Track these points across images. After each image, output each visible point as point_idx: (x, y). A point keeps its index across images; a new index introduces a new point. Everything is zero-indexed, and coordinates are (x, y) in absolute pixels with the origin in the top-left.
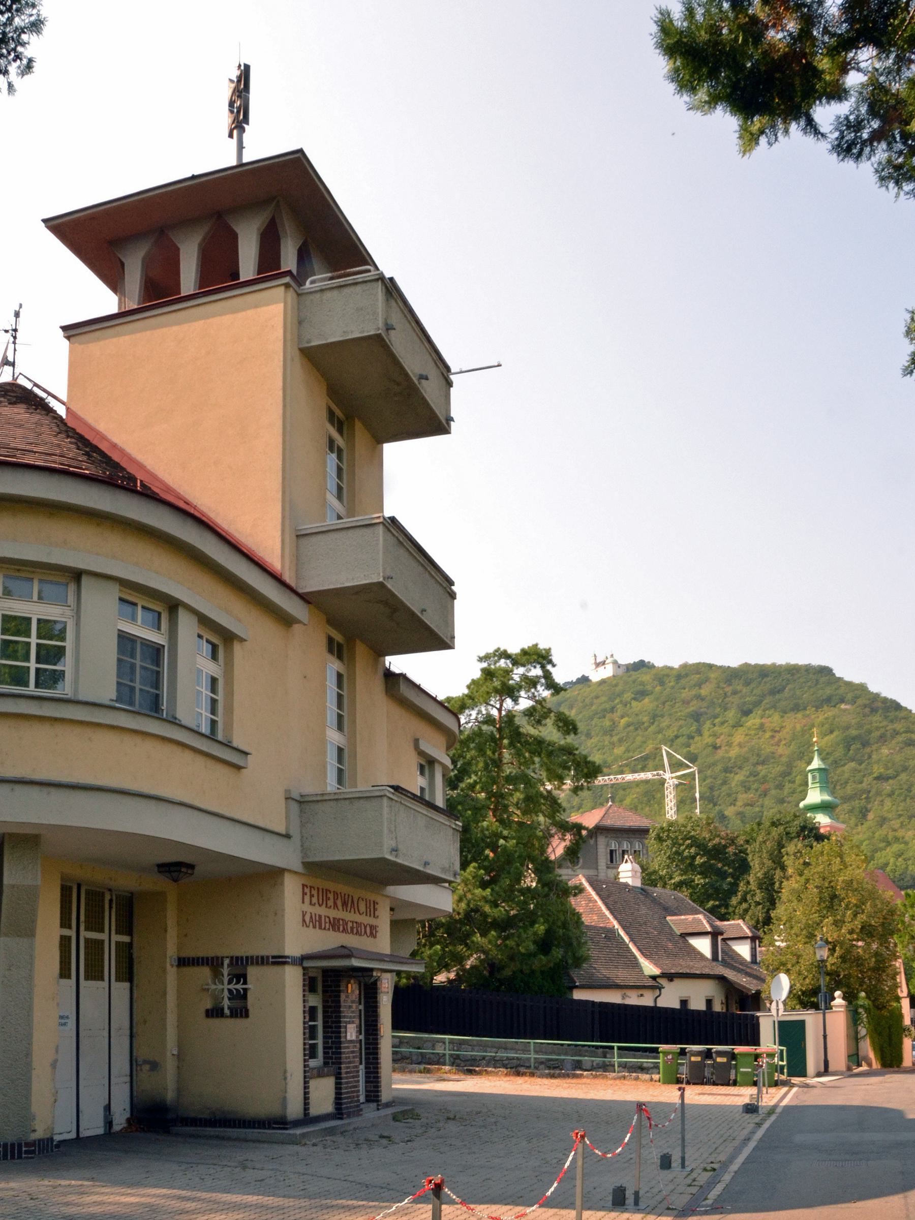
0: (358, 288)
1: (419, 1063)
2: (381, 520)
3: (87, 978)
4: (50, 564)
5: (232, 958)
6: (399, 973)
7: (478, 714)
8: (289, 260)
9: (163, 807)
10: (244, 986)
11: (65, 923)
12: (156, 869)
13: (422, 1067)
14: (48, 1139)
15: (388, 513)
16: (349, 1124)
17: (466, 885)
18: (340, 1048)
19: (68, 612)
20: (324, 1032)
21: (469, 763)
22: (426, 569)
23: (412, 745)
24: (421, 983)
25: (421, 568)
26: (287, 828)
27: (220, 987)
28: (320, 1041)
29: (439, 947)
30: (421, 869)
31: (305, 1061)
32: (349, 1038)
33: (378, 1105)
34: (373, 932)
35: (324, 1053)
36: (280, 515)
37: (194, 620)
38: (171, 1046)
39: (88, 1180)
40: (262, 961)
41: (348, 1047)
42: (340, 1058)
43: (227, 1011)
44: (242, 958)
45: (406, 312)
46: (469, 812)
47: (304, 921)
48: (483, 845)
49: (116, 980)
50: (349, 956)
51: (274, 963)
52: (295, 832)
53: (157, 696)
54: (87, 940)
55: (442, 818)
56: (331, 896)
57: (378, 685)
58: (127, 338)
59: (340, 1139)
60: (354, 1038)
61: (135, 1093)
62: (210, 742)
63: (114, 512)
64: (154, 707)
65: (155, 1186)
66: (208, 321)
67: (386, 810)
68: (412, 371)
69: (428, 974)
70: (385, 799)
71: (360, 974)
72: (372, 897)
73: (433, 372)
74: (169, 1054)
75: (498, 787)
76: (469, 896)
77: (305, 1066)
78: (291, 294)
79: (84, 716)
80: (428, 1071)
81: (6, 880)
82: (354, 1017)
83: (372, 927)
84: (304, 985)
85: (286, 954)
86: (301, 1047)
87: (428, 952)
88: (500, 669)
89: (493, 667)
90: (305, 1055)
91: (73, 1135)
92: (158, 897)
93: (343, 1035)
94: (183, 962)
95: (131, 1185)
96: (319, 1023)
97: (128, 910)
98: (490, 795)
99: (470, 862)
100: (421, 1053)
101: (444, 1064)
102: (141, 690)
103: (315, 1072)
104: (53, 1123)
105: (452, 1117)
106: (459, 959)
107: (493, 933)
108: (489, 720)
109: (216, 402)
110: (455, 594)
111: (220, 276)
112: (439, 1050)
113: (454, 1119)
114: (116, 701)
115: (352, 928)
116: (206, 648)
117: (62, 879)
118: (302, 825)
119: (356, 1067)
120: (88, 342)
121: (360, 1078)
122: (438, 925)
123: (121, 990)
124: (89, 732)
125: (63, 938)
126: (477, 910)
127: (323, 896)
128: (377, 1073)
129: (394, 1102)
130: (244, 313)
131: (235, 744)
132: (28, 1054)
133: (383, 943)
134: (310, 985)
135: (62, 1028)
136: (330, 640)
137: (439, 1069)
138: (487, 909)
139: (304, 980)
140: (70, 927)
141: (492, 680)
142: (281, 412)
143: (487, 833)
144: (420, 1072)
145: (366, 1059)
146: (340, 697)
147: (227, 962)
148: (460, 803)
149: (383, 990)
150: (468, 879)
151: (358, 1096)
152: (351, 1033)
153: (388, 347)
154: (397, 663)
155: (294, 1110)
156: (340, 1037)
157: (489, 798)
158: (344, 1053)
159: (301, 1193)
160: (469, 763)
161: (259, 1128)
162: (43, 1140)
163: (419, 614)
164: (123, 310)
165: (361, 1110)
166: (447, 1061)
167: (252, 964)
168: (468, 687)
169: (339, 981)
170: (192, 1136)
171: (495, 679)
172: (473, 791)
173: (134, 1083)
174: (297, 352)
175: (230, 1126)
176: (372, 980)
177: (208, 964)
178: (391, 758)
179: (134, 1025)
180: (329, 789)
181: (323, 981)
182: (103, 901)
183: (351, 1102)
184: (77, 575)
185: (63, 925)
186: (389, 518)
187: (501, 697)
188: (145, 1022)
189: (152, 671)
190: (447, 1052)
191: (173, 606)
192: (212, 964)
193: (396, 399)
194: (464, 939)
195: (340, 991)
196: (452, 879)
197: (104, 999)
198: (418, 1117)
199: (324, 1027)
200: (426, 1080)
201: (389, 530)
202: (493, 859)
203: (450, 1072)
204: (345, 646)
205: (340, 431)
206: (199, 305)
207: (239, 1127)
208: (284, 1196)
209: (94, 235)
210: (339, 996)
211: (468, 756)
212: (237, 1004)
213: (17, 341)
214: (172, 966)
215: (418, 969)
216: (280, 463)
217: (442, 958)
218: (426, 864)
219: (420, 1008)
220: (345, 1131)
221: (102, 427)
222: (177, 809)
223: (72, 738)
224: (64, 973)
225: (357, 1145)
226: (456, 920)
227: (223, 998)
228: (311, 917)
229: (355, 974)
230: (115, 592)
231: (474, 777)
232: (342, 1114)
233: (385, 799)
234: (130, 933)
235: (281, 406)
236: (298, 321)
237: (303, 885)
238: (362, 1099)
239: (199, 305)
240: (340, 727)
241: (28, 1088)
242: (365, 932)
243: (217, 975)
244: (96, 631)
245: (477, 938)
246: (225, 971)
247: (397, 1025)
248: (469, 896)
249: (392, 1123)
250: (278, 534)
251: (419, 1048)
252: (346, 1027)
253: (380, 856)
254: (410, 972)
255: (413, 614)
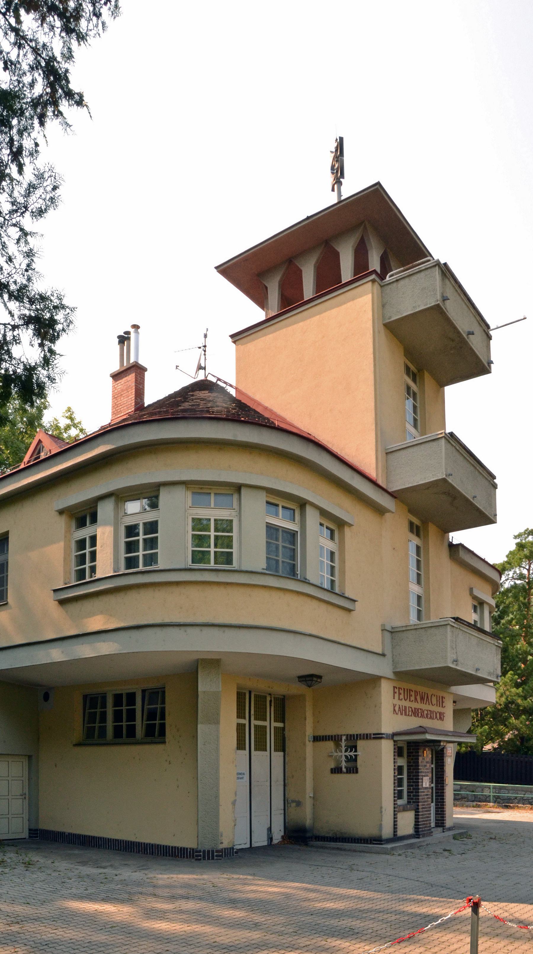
0: (423, 274)
1: (473, 801)
2: (443, 435)
3: (256, 749)
4: (221, 482)
5: (347, 735)
6: (460, 744)
7: (514, 574)
8: (375, 264)
9: (299, 637)
10: (355, 753)
11: (240, 714)
12: (297, 679)
13: (475, 803)
14: (230, 848)
15: (448, 431)
16: (424, 841)
17: (506, 686)
18: (418, 792)
19: (234, 513)
20: (408, 782)
21: (508, 607)
22: (476, 468)
23: (468, 593)
24: (475, 750)
25: (472, 468)
26: (383, 649)
27: (340, 754)
28: (405, 788)
29: (487, 727)
30: (474, 673)
31: (395, 801)
32: (424, 786)
33: (443, 829)
34: (441, 716)
35: (408, 796)
36: (374, 440)
37: (317, 513)
38: (309, 792)
39: (251, 875)
40: (367, 737)
41: (424, 792)
42: (418, 799)
43: (344, 770)
44: (354, 735)
45: (457, 287)
46: (508, 639)
47: (394, 710)
48: (517, 659)
49: (275, 751)
50: (424, 733)
51: (374, 738)
52: (388, 652)
53: (294, 565)
54: (256, 726)
55: (488, 639)
56: (413, 694)
57: (445, 553)
58: (271, 336)
59: (417, 851)
60: (428, 786)
61: (287, 820)
62: (329, 594)
63: (260, 443)
64: (292, 572)
65: (293, 881)
66: (322, 315)
67: (449, 634)
68: (462, 329)
69: (479, 744)
70: (449, 627)
71: (432, 744)
72: (441, 694)
73: (477, 330)
74: (307, 796)
75: (527, 621)
76: (508, 693)
77: (394, 804)
78: (376, 286)
79: (248, 582)
80: (479, 806)
81: (200, 689)
82: (428, 772)
83: (440, 713)
84: (394, 752)
85: (382, 732)
86: (392, 792)
87: (479, 730)
88: (529, 542)
89: (524, 541)
90: (394, 797)
91: (248, 846)
92: (300, 698)
93: (420, 784)
94: (316, 739)
95: (278, 879)
96: (405, 776)
97: (282, 706)
98: (522, 626)
99: (509, 671)
100: (474, 795)
101: (489, 802)
102: (283, 562)
103: (401, 808)
104: (234, 839)
105: (494, 837)
106: (501, 735)
107: (523, 716)
108: (521, 577)
109: (328, 371)
110: (497, 485)
111: (330, 283)
112: (486, 793)
113: (495, 839)
114: (266, 569)
115: (427, 714)
116: (326, 533)
117: (238, 688)
118: (393, 647)
119: (429, 804)
120: (247, 343)
121: (432, 812)
122: (487, 713)
123: (278, 757)
124: (248, 591)
125: (238, 725)
126: (512, 702)
127: (408, 694)
128: (443, 808)
129: (454, 827)
130: (345, 305)
131: (346, 595)
132: (217, 797)
133: (448, 724)
134: (399, 752)
135: (240, 780)
136: (411, 524)
137: (486, 805)
138: (519, 701)
139: (395, 749)
140: (245, 718)
141: (523, 550)
142: (373, 369)
143: (520, 652)
144: (474, 807)
145: (436, 799)
146: (418, 562)
147: (344, 738)
148: (501, 633)
149: (448, 754)
150: (507, 682)
151: (430, 823)
152: (426, 782)
153: (445, 313)
154: (457, 537)
155: (387, 832)
156: (418, 785)
157: (521, 629)
158: (421, 796)
159: (387, 888)
160: (508, 607)
161: (364, 843)
162: (228, 849)
163: (471, 500)
164: (268, 317)
165: (432, 832)
166: (492, 800)
167: (360, 739)
168: (507, 556)
169: (418, 749)
170: (322, 847)
171: (525, 549)
172: (510, 625)
173: (286, 815)
174: (382, 328)
175: (345, 842)
176: (441, 748)
177: (332, 740)
178: (452, 600)
179: (286, 779)
180: (412, 623)
181: (408, 749)
182: (266, 702)
183: (425, 827)
184: (238, 488)
185: (239, 717)
186: (449, 433)
187: (529, 561)
188: (293, 776)
189: (290, 549)
190: (492, 794)
191: (303, 504)
192: (335, 740)
193: (452, 352)
194: (504, 722)
195: (418, 756)
196: (495, 680)
197: (267, 763)
198: (470, 837)
199: (408, 779)
200: (477, 812)
201: (449, 442)
202: (524, 669)
203: (493, 807)
204: (421, 528)
205: (414, 380)
206: (316, 305)
207: (352, 842)
208: (375, 891)
209: (249, 272)
210: (418, 759)
211: (507, 602)
212: (350, 765)
213: (206, 353)
214: (309, 741)
215: (471, 740)
216: (373, 404)
217: (489, 734)
218: (477, 670)
219: (473, 766)
220: (420, 846)
221: (257, 397)
222: (308, 638)
223: (237, 594)
224: (240, 746)
225: (428, 855)
226: (499, 710)
227: (342, 761)
228: (399, 708)
229: (428, 744)
230: (263, 497)
231: (511, 616)
232: (419, 835)
233: (449, 627)
234: (283, 721)
235: (372, 366)
236: (382, 305)
237: (394, 687)
238: (433, 825)
239: (316, 305)
240: (419, 582)
241: (217, 816)
242: (436, 717)
243: (338, 746)
244: (252, 525)
245: (513, 720)
246: (343, 744)
247: (457, 776)
248: (508, 693)
249: (453, 841)
250: (373, 454)
251: (473, 792)
252: (422, 779)
253: (445, 665)
254: (467, 743)
255: (467, 500)
